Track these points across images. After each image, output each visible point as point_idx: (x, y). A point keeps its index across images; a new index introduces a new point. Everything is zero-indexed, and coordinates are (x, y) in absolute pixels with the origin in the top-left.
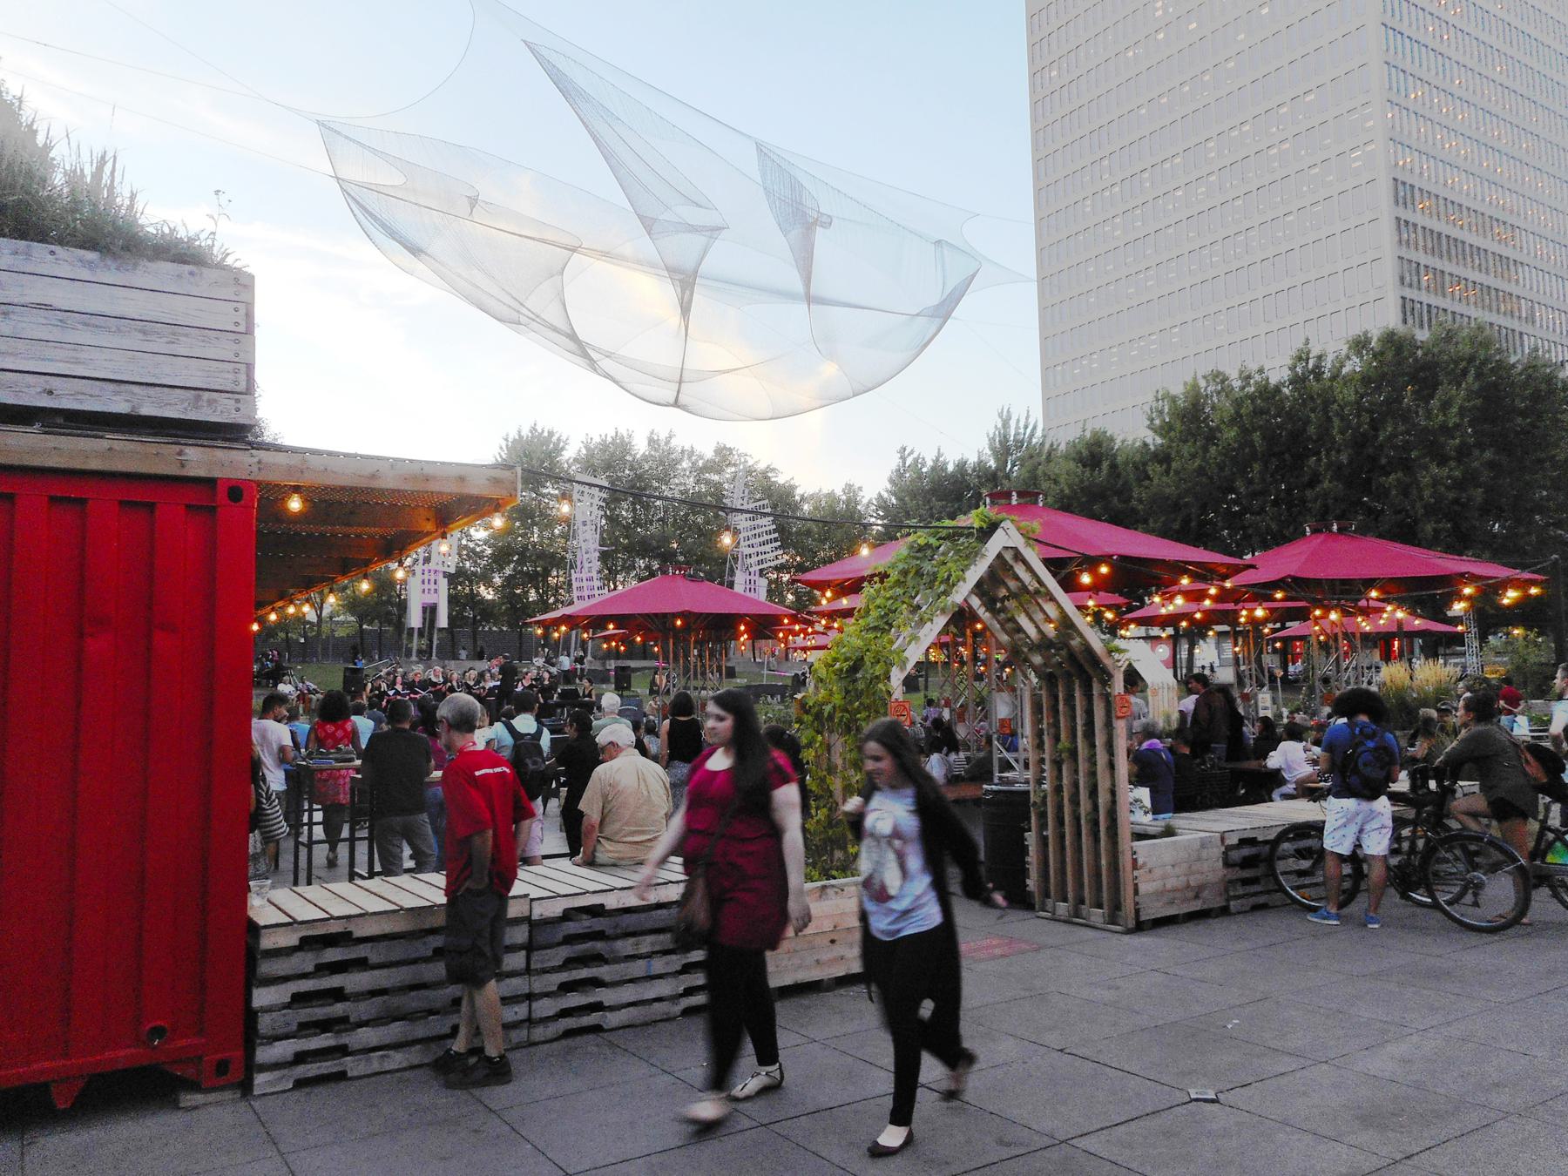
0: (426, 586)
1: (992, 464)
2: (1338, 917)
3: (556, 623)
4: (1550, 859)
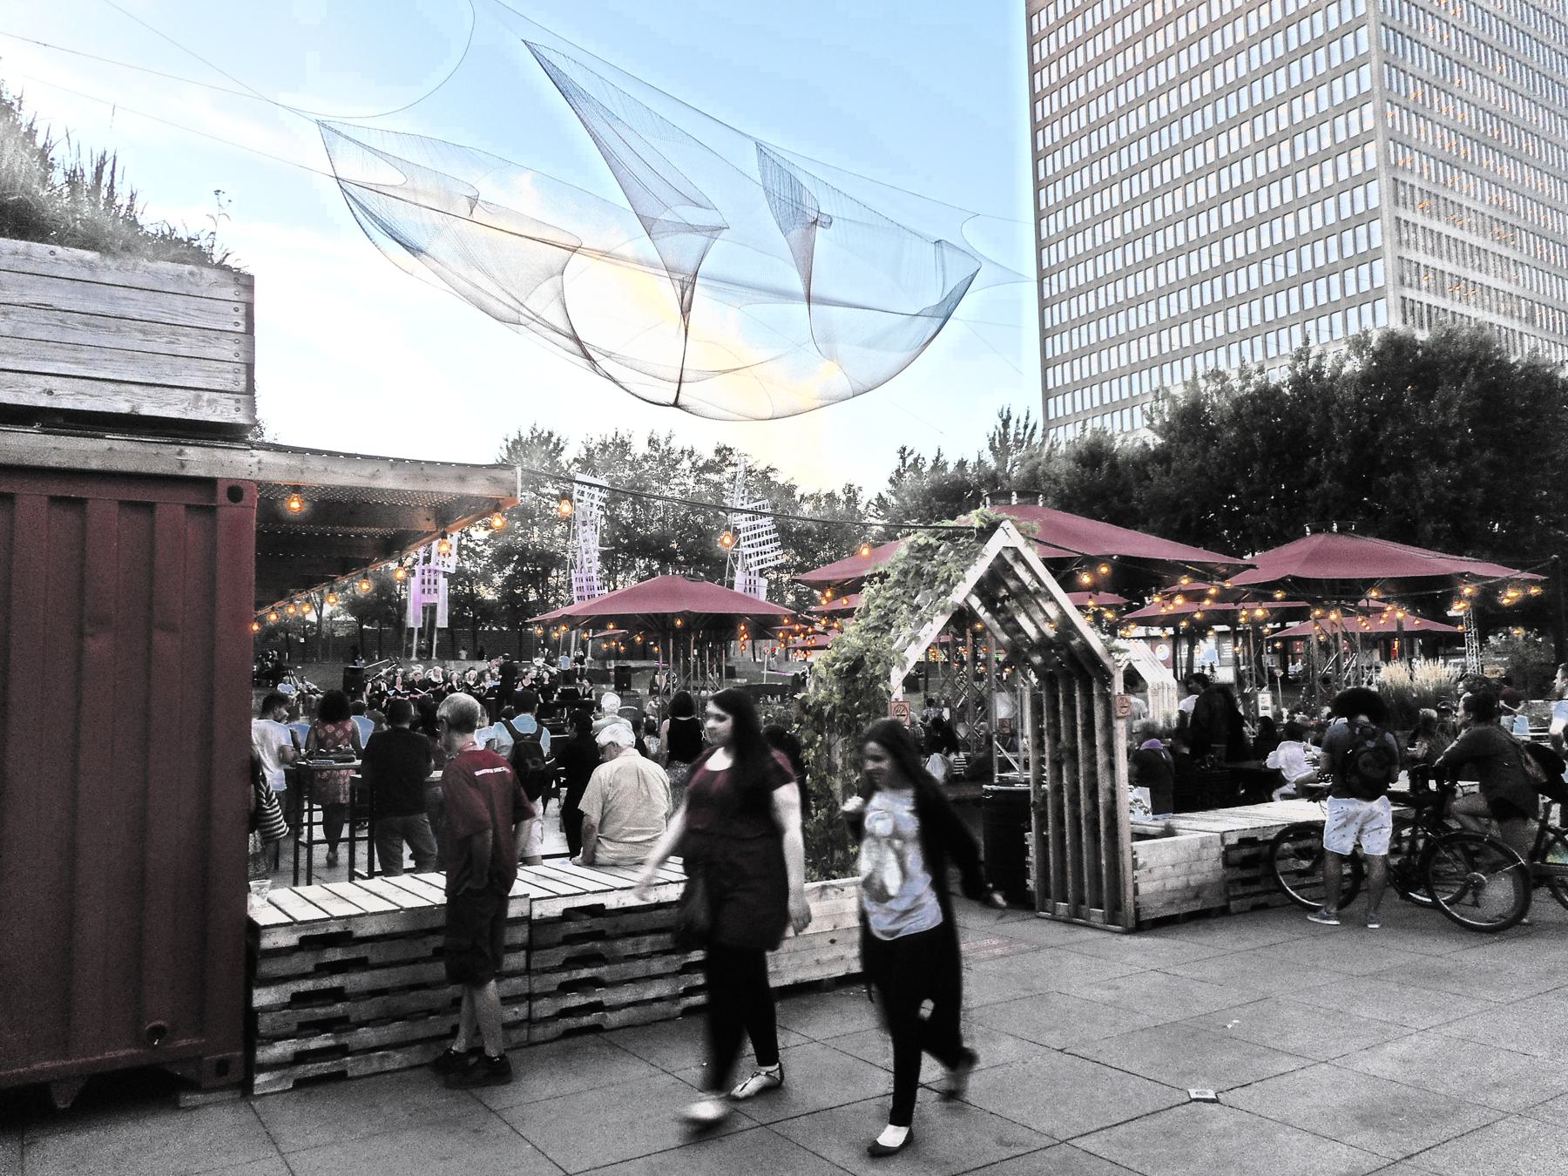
0: (426, 586)
1: (992, 463)
2: (1338, 917)
3: (556, 622)
4: (1550, 859)
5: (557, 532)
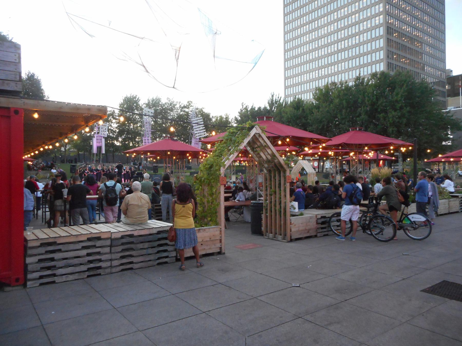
0: (98, 141)
1: (268, 108)
2: (344, 238)
3: (133, 152)
4: (404, 222)
5: (138, 125)
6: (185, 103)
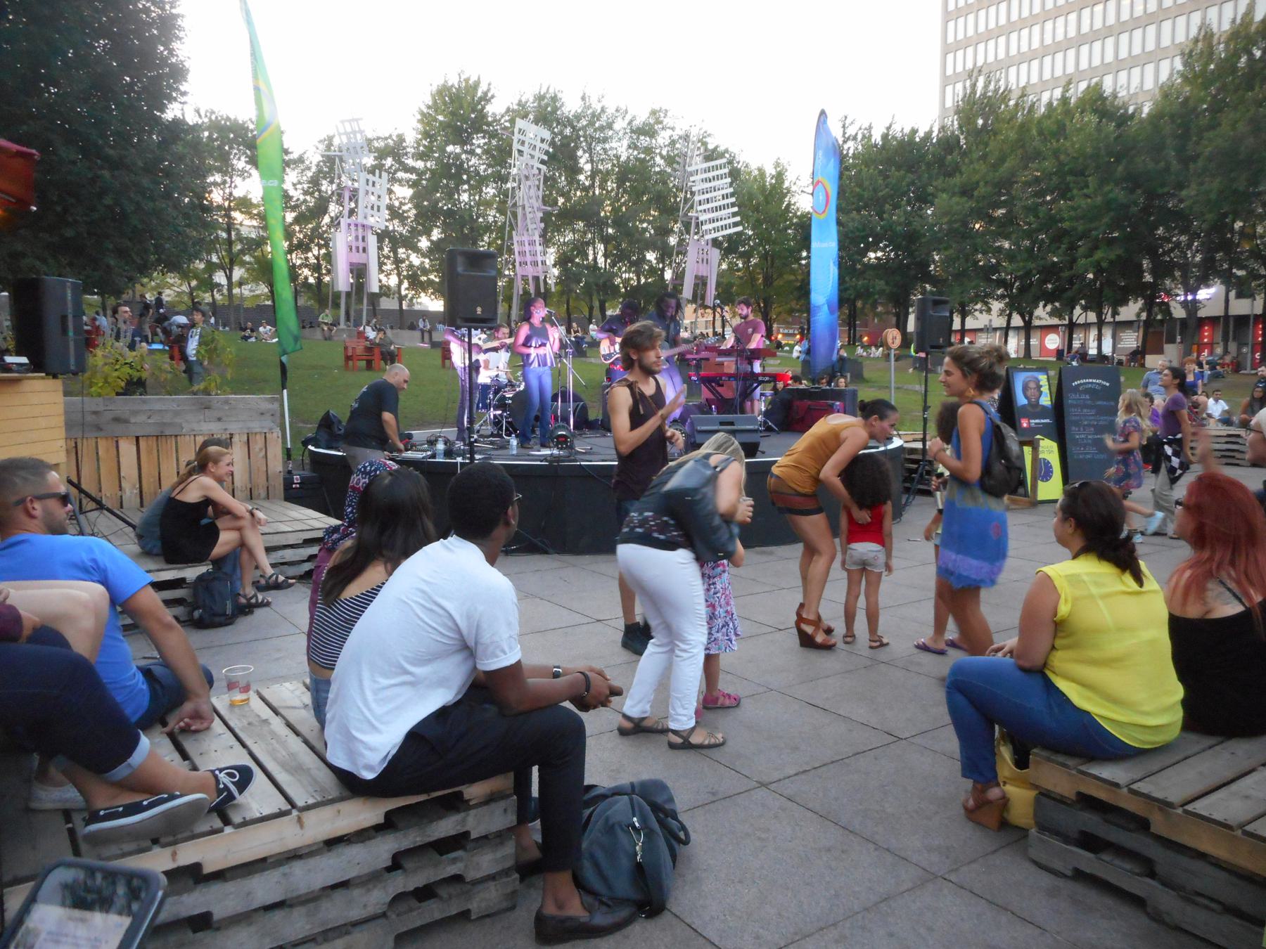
6: (642, 117)
